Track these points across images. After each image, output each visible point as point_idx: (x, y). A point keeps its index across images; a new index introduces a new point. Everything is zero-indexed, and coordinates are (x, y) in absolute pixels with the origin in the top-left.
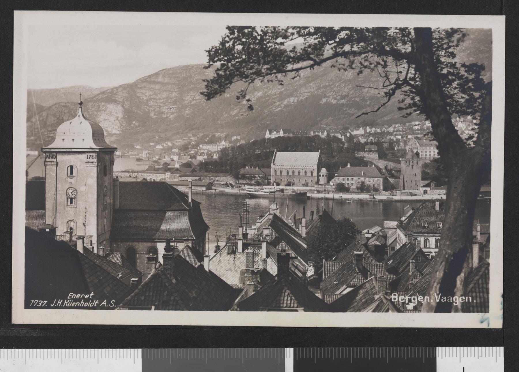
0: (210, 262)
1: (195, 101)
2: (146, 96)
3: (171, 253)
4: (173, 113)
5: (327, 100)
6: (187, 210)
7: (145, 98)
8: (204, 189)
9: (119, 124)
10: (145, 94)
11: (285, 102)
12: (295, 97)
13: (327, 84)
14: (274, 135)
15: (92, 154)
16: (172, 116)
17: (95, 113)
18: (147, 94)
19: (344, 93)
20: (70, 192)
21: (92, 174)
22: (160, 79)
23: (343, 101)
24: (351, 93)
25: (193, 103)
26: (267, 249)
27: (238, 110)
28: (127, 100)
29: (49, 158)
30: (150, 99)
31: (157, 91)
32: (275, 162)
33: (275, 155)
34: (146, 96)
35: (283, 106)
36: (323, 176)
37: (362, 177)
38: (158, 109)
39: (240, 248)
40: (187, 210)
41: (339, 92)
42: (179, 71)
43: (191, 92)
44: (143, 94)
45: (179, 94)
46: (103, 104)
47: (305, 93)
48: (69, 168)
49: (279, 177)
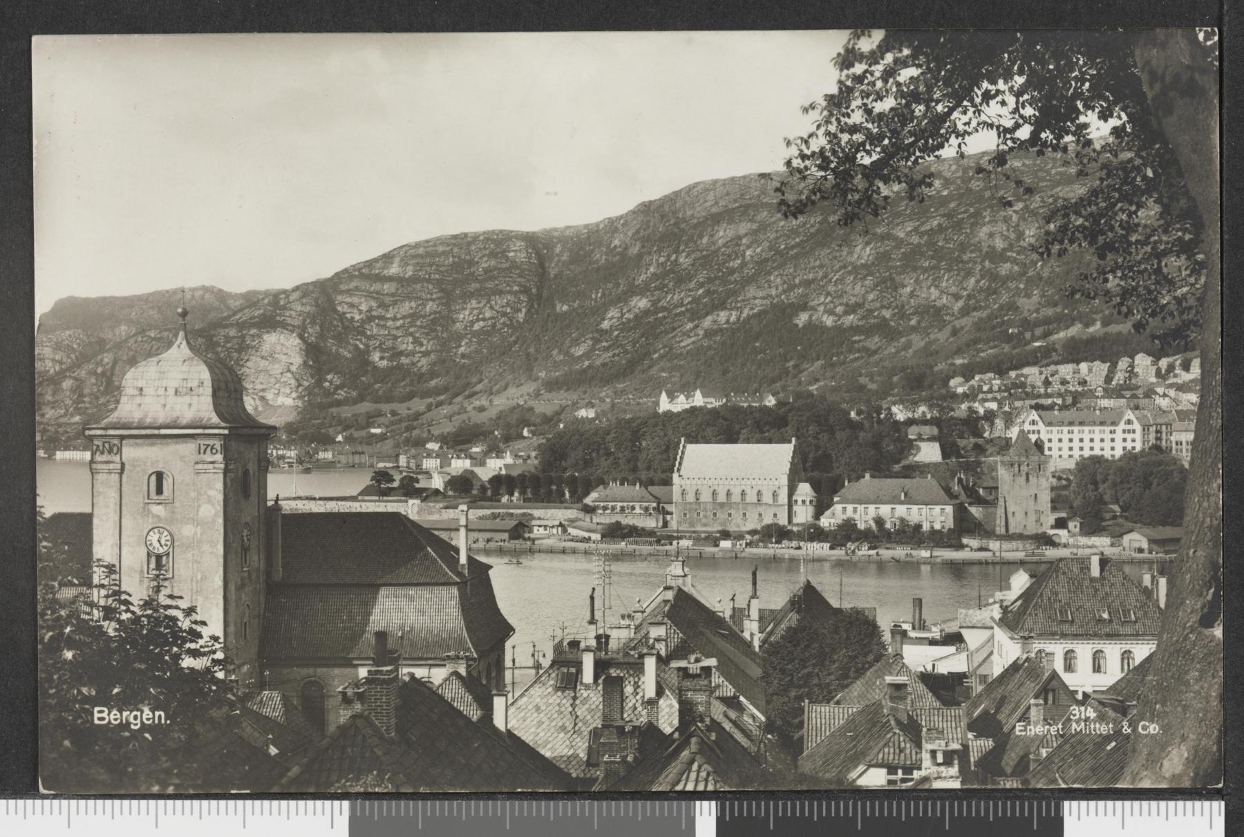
0: (512, 710)
1: (481, 323)
2: (360, 312)
3: (389, 668)
4: (426, 354)
5: (811, 316)
6: (455, 584)
7: (357, 317)
8: (506, 536)
9: (293, 382)
10: (355, 307)
11: (707, 322)
12: (731, 309)
13: (811, 276)
14: (680, 404)
15: (211, 442)
16: (424, 361)
17: (235, 355)
18: (364, 308)
19: (853, 300)
20: (154, 537)
21: (212, 493)
22: (394, 270)
23: (850, 319)
24: (871, 297)
25: (476, 327)
26: (658, 675)
27: (590, 343)
28: (313, 323)
29: (102, 453)
30: (370, 319)
31: (388, 300)
32: (682, 472)
33: (683, 453)
34: (360, 312)
35: (701, 333)
36: (804, 502)
37: (902, 503)
38: (389, 343)
39: (588, 675)
40: (455, 584)
41: (841, 296)
42: (441, 249)
43: (474, 302)
44: (352, 305)
45: (443, 304)
46: (253, 331)
47: (755, 298)
48: (154, 478)
49: (694, 506)
